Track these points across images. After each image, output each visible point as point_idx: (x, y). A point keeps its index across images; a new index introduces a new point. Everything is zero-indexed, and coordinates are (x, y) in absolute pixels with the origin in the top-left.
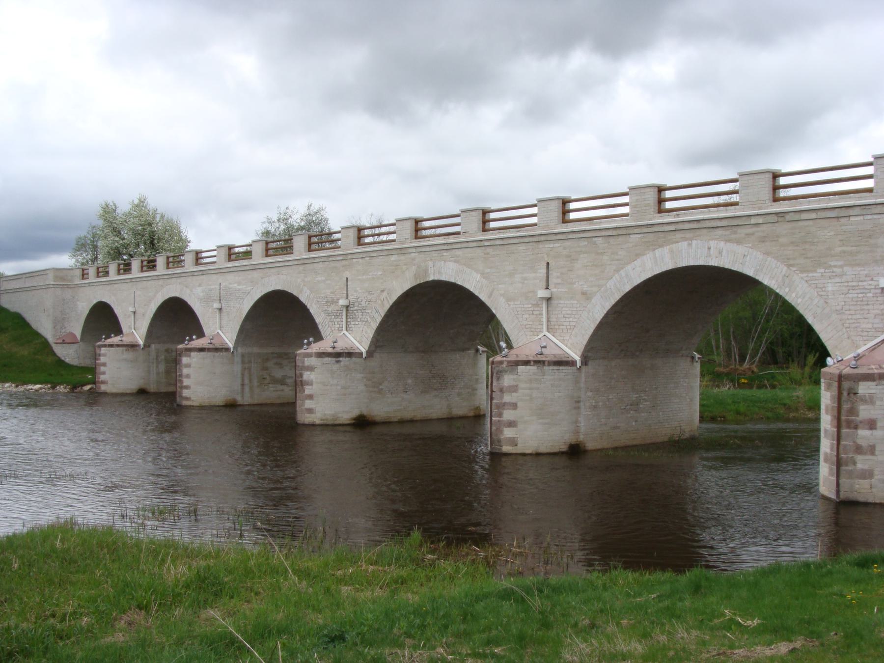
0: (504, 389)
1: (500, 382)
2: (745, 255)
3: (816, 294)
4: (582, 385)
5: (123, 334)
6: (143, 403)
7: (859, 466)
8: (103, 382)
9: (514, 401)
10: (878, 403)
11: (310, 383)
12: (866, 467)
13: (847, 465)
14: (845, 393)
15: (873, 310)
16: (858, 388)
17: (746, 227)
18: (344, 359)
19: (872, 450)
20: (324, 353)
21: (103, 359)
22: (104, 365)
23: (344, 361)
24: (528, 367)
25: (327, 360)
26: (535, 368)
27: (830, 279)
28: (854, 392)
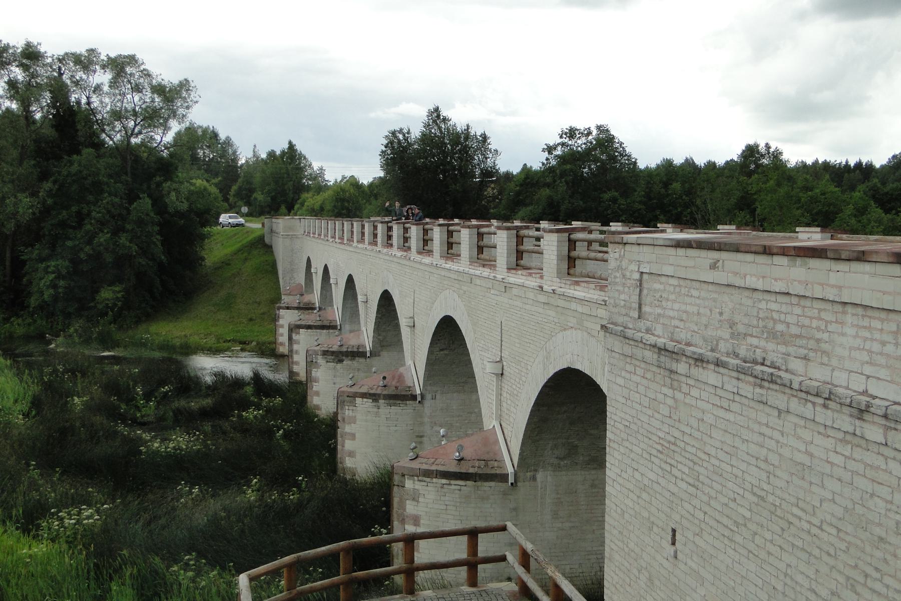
10: (421, 500)
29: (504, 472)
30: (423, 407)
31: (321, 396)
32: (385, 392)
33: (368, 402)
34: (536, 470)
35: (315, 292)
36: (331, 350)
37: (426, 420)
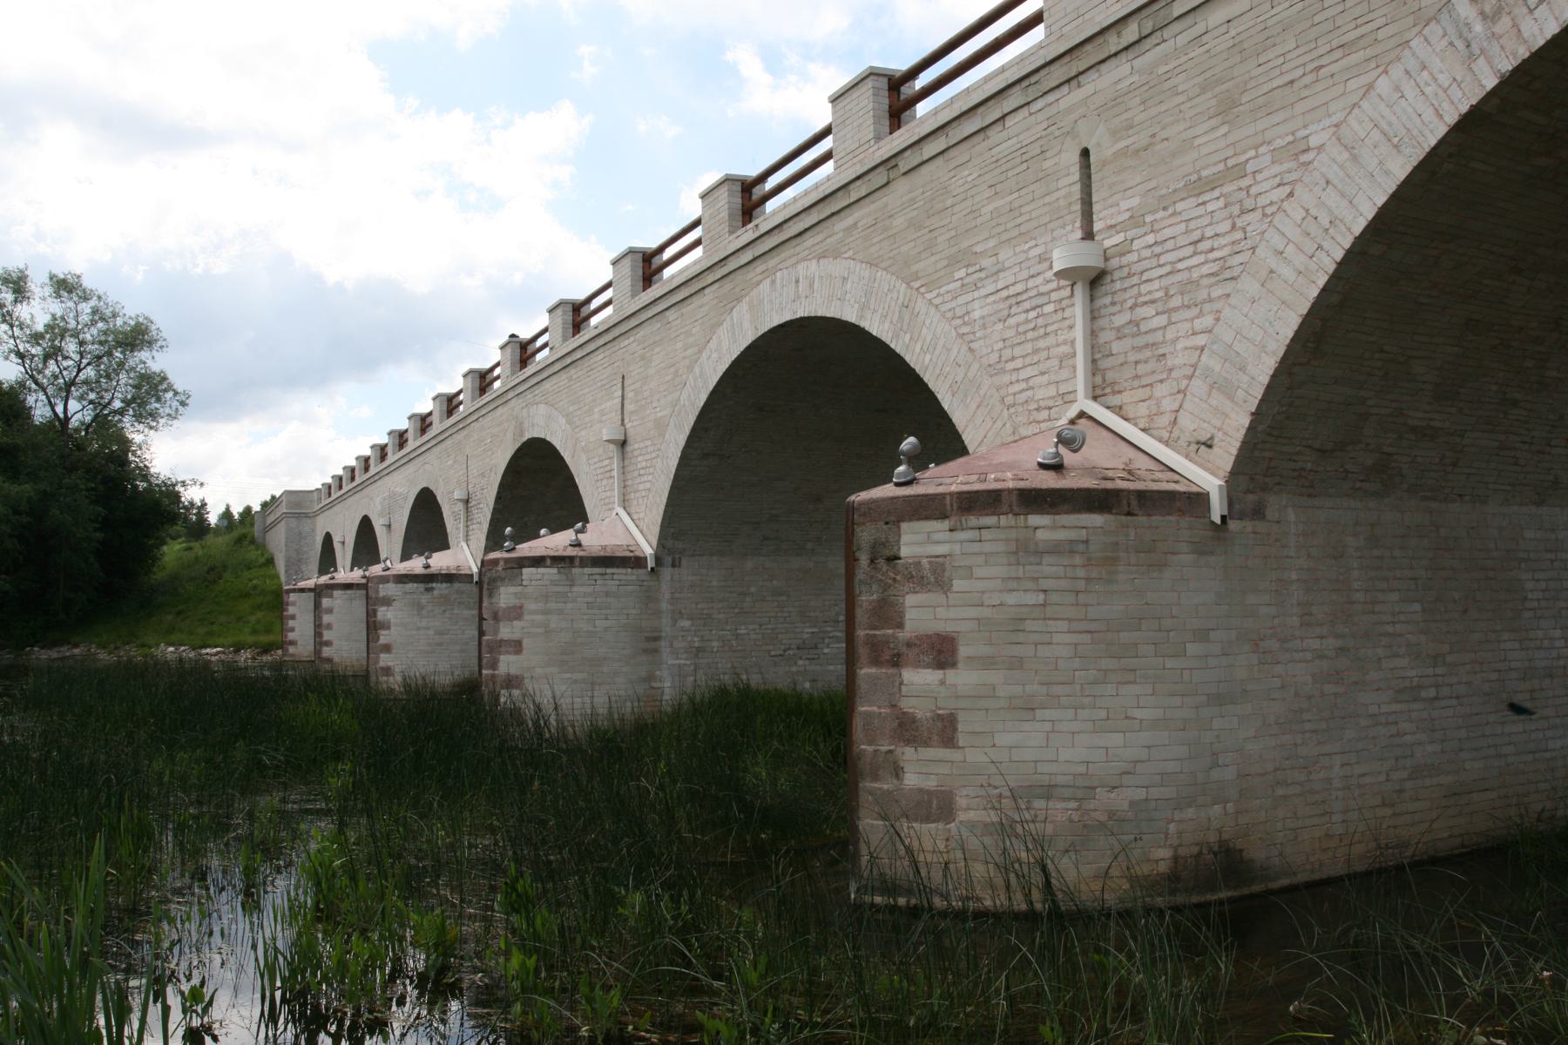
0: (500, 614)
1: (494, 601)
2: (844, 278)
3: (954, 333)
4: (664, 606)
6: (707, 695)
7: (911, 780)
8: (293, 643)
9: (516, 636)
10: (958, 584)
11: (386, 626)
12: (931, 784)
13: (876, 778)
14: (864, 559)
15: (1058, 345)
16: (898, 541)
17: (842, 214)
18: (439, 585)
19: (945, 730)
21: (291, 610)
22: (293, 617)
23: (440, 588)
24: (541, 570)
25: (410, 586)
26: (554, 571)
27: (977, 288)
28: (887, 553)
30: (658, 580)
31: (394, 651)
37: (664, 606)
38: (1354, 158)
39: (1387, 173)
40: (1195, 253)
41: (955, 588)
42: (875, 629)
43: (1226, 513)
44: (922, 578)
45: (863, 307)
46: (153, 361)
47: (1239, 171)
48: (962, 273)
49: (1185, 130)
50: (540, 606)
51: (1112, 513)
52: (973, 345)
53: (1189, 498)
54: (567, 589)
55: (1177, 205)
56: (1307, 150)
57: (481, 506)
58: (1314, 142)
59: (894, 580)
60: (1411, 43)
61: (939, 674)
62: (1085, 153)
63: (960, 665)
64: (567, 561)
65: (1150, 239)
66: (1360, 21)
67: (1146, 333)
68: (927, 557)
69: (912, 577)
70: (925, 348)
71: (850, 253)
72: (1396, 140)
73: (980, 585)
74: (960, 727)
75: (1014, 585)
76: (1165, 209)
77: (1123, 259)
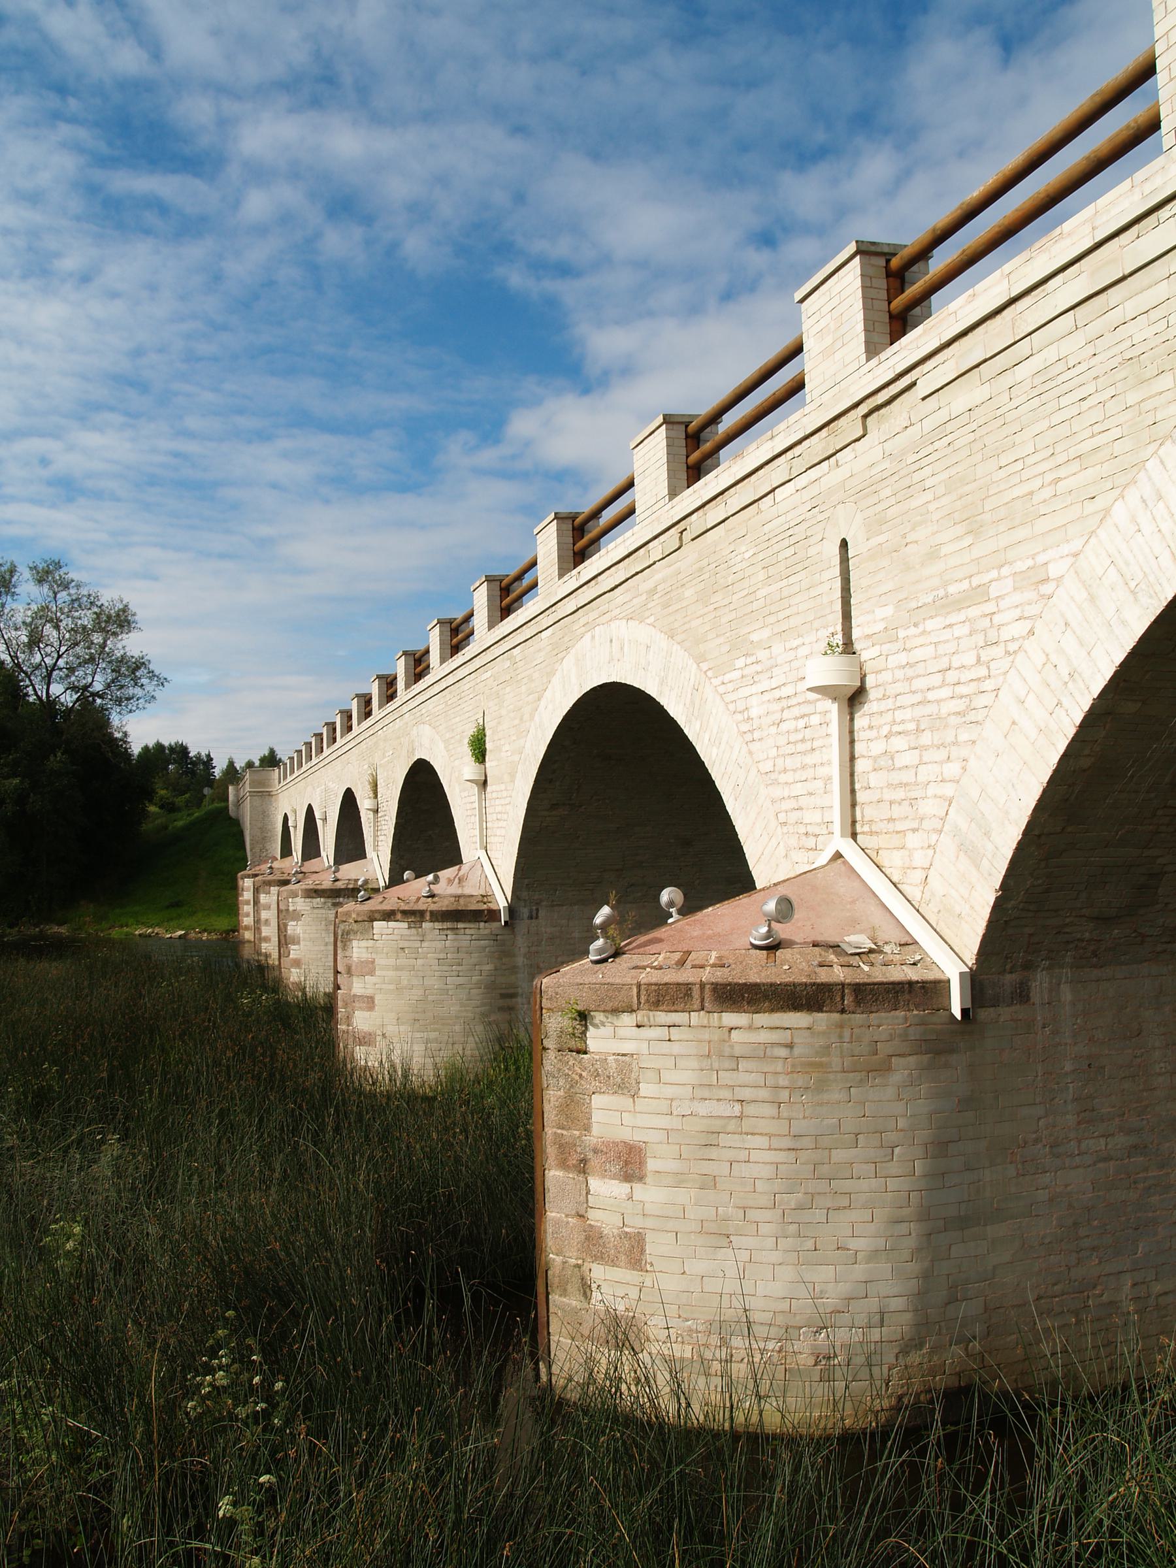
4: (520, 961)
5: (460, 862)
9: (369, 992)
10: (645, 1089)
11: (296, 941)
13: (564, 1293)
20: (316, 891)
24: (392, 924)
25: (319, 901)
29: (930, 976)
30: (513, 932)
32: (433, 907)
33: (399, 927)
34: (1028, 966)
35: (294, 854)
36: (319, 887)
37: (520, 961)
38: (1092, 599)
39: (1124, 623)
40: (944, 684)
41: (642, 1093)
42: (563, 1129)
43: (969, 1005)
44: (609, 1077)
45: (662, 682)
46: (130, 644)
47: (980, 594)
48: (740, 663)
49: (933, 534)
50: (392, 962)
51: (822, 1012)
52: (755, 747)
53: (923, 987)
54: (418, 944)
55: (927, 622)
56: (1046, 580)
57: (386, 818)
58: (1054, 571)
59: (581, 1076)
60: (1148, 464)
61: (626, 1187)
62: (844, 544)
63: (648, 1180)
64: (418, 915)
65: (903, 658)
66: (1097, 428)
67: (900, 769)
68: (614, 1054)
69: (598, 1075)
70: (712, 740)
71: (651, 619)
72: (1132, 585)
73: (669, 1091)
74: (648, 1249)
75: (706, 1093)
76: (916, 625)
77: (879, 676)
